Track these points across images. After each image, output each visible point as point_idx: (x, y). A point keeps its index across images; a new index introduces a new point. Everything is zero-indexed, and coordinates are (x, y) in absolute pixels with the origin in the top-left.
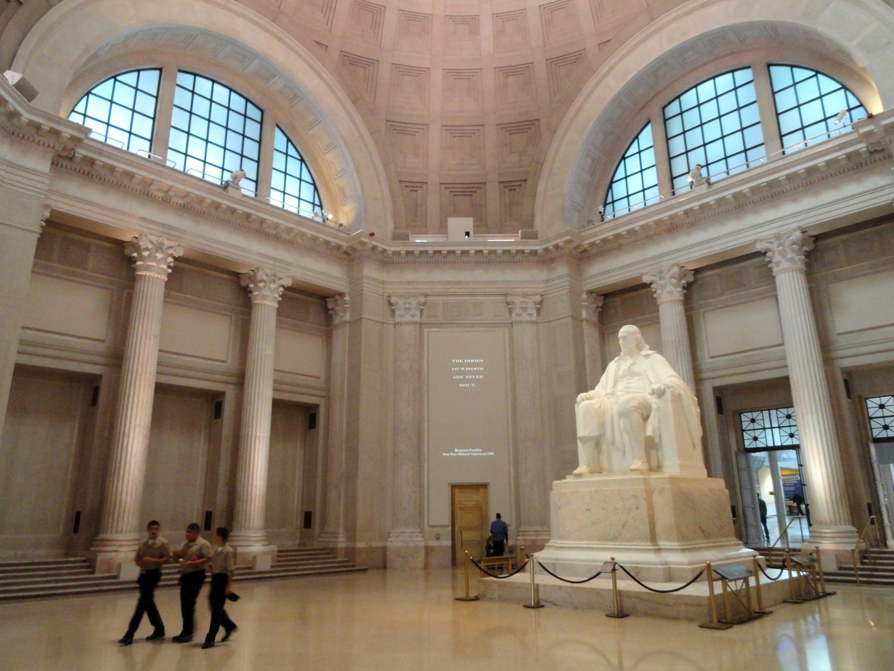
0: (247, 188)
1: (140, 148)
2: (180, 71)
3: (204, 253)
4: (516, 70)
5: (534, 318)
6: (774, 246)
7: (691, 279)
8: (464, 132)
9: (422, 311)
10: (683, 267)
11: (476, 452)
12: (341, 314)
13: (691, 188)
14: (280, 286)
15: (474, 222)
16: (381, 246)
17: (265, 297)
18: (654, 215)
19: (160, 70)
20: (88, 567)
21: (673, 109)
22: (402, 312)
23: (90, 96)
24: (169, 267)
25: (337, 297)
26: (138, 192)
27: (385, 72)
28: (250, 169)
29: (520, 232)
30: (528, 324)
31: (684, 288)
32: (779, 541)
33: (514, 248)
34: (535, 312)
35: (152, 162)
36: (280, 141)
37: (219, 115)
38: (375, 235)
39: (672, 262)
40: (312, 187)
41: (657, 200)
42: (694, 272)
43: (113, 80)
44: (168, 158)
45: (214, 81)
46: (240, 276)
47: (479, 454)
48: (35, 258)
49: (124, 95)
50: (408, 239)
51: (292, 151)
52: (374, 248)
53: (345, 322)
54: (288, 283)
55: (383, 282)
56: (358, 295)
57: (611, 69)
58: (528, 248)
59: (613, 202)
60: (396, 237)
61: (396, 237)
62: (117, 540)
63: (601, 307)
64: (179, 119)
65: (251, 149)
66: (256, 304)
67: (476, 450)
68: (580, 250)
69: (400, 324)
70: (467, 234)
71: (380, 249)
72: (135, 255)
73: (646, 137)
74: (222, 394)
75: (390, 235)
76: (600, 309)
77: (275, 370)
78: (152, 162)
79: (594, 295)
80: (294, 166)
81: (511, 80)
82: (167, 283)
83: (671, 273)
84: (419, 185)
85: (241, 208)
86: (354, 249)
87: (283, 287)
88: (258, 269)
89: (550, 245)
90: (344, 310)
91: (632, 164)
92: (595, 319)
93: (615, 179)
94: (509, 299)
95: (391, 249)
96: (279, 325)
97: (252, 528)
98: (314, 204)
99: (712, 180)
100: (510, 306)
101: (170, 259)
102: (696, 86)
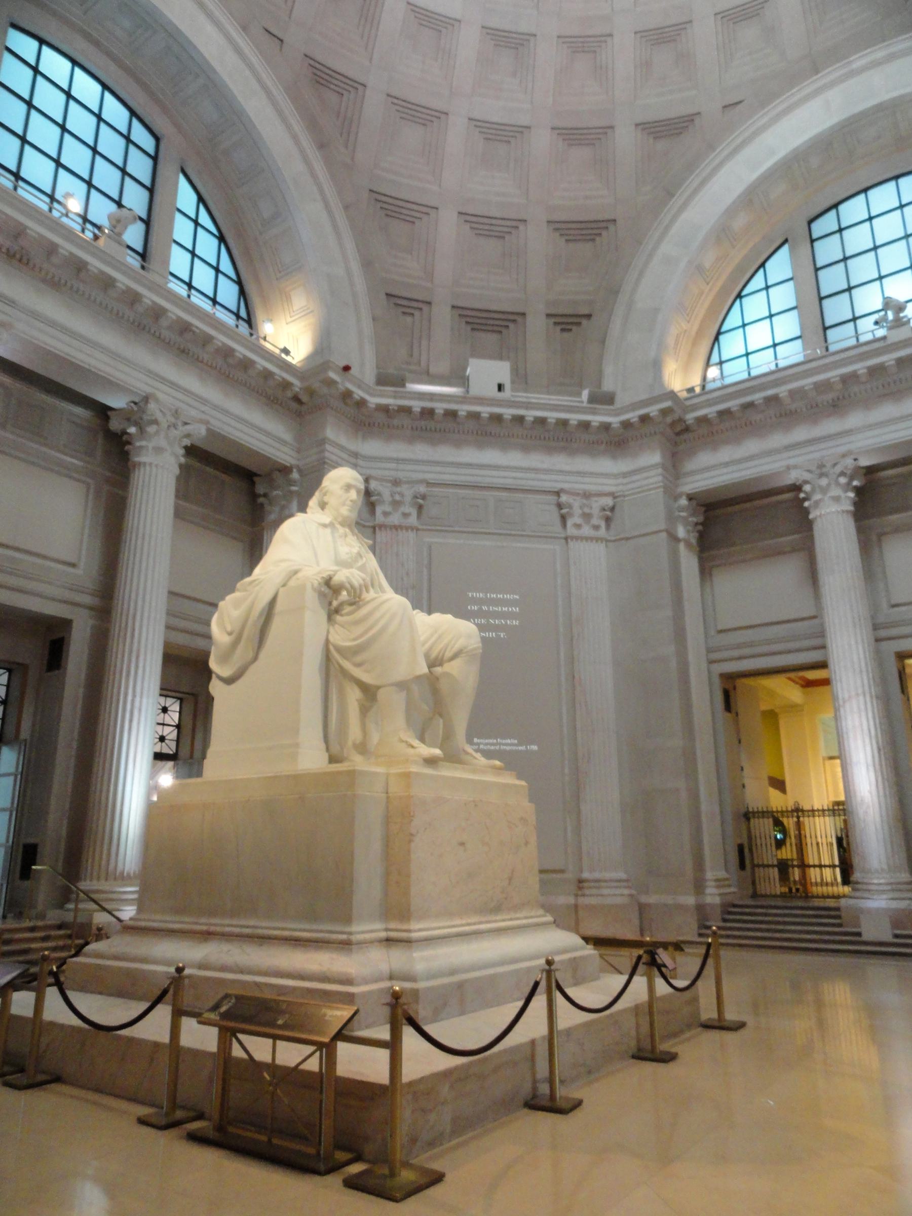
5: (602, 532)
8: (492, 228)
12: (283, 503)
16: (358, 393)
17: (159, 450)
18: (812, 375)
21: (827, 223)
22: (388, 509)
25: (276, 475)
32: (245, 1056)
33: (574, 418)
36: (186, 198)
41: (799, 358)
45: (75, 63)
46: (109, 413)
47: (514, 748)
50: (404, 386)
51: (204, 219)
52: (347, 395)
58: (596, 419)
59: (721, 363)
60: (382, 380)
61: (382, 380)
63: (702, 524)
65: (135, 199)
67: (509, 741)
68: (678, 429)
69: (382, 526)
76: (700, 528)
79: (694, 503)
80: (208, 246)
83: (838, 469)
86: (311, 393)
88: (146, 399)
89: (633, 416)
91: (754, 306)
92: (694, 541)
93: (724, 329)
94: (564, 498)
102: (865, 190)
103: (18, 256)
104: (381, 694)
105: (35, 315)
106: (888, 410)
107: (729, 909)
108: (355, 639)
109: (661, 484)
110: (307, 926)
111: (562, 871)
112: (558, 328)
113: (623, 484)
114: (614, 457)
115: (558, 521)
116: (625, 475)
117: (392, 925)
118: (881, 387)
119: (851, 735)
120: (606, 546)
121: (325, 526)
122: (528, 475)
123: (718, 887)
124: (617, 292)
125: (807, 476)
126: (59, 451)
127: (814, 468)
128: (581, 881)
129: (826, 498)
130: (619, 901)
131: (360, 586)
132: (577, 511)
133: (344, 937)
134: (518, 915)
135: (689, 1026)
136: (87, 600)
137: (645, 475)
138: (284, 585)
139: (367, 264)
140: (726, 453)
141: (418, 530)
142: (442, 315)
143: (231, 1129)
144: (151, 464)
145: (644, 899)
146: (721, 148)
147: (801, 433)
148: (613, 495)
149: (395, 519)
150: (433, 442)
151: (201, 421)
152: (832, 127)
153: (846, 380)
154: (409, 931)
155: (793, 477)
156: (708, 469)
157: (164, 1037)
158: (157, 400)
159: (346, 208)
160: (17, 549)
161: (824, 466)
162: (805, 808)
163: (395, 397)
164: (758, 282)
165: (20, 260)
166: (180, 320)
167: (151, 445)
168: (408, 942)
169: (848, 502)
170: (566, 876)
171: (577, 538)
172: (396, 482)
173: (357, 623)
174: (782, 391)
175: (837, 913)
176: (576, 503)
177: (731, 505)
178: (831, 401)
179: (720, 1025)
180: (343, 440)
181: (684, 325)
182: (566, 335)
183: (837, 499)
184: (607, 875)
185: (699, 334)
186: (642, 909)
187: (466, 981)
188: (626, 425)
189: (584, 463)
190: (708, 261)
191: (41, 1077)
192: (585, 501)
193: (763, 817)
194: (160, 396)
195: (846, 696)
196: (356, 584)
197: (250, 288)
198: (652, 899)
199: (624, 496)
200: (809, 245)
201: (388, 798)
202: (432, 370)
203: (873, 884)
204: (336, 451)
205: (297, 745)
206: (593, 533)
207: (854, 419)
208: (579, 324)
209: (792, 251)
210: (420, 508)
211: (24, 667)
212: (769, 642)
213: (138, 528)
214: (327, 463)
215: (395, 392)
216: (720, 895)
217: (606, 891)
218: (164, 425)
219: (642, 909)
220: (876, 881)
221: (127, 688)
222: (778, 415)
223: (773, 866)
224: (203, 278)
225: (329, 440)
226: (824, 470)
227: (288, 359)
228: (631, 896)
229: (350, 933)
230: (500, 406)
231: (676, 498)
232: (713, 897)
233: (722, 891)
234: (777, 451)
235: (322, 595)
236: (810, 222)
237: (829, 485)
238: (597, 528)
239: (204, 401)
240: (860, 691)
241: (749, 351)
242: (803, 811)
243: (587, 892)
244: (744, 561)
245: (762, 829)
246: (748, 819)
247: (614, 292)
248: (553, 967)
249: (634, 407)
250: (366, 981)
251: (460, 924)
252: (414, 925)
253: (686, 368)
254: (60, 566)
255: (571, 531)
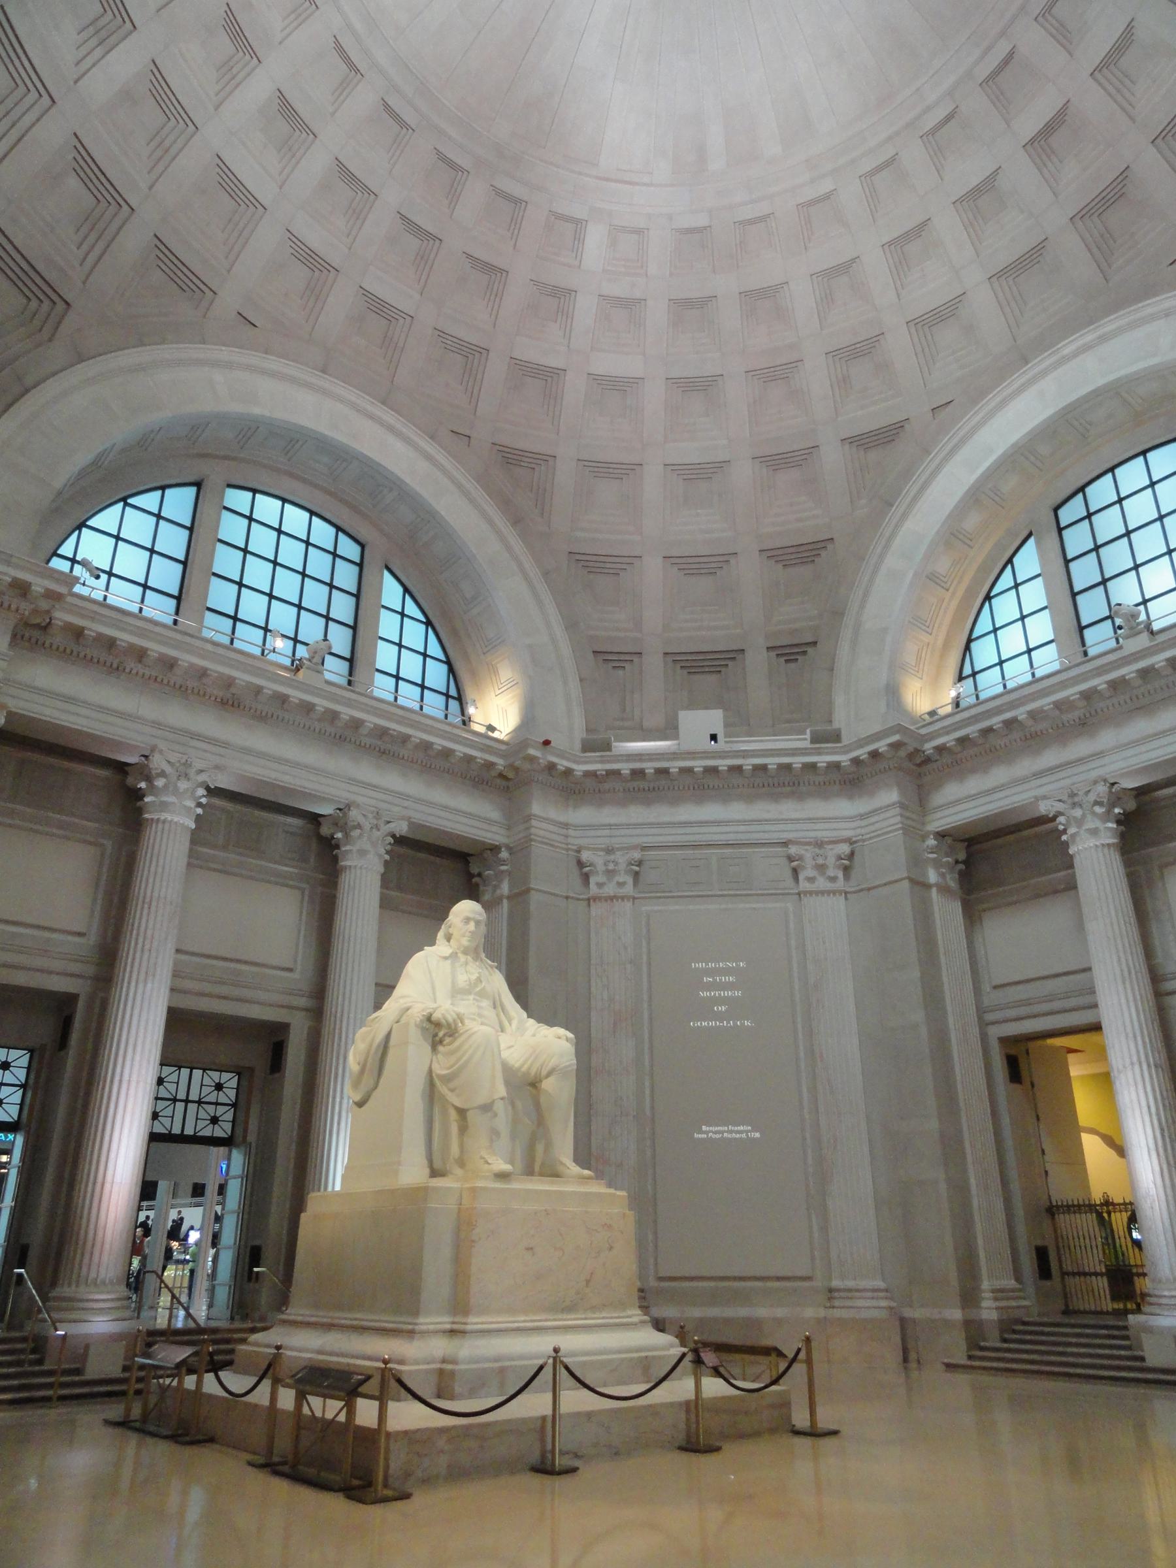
0: (335, 669)
1: (159, 609)
2: (230, 486)
3: (253, 778)
4: (95, 181)
5: (840, 884)
6: (367, 826)
7: (1131, 805)
9: (637, 874)
10: (1113, 784)
11: (742, 1131)
13: (1118, 642)
14: (386, 836)
15: (725, 717)
16: (563, 764)
17: (362, 853)
19: (198, 485)
20: (33, 1351)
23: (84, 530)
24: (199, 805)
26: (213, 698)
27: (565, 475)
28: (340, 639)
29: (808, 731)
30: (829, 895)
31: (1119, 822)
32: (310, 1413)
33: (797, 761)
34: (840, 875)
35: (181, 632)
36: (391, 592)
37: (291, 553)
38: (552, 744)
39: (1094, 774)
40: (445, 668)
41: (1056, 666)
42: (1134, 793)
43: (121, 504)
44: (205, 624)
45: (312, 513)
48: (382, 887)
49: (137, 526)
51: (411, 609)
52: (551, 767)
53: (501, 898)
54: (402, 828)
55: (566, 826)
56: (521, 850)
57: (230, 365)
58: (822, 760)
59: (974, 674)
60: (587, 747)
61: (587, 747)
62: (88, 1300)
63: (964, 862)
64: (226, 561)
65: (343, 608)
66: (345, 867)
69: (596, 899)
70: (714, 737)
71: (578, 773)
72: (143, 785)
73: (1028, 561)
74: (283, 1028)
75: (578, 745)
76: (962, 866)
77: (377, 984)
78: (181, 632)
79: (949, 840)
80: (415, 634)
81: (73, 182)
82: (194, 833)
83: (1092, 797)
84: (627, 657)
85: (321, 703)
87: (393, 836)
88: (348, 806)
89: (862, 753)
90: (499, 875)
91: (1006, 608)
92: (953, 885)
94: (793, 850)
95: (580, 768)
96: (385, 903)
97: (95, 1283)
98: (447, 696)
99: (1156, 626)
100: (795, 863)
101: (201, 791)
103: (230, 702)
104: (470, 1114)
105: (247, 751)
106: (1141, 726)
107: (1010, 1327)
108: (449, 1068)
109: (900, 825)
110: (392, 1319)
111: (809, 1278)
112: (782, 660)
113: (861, 827)
114: (851, 797)
115: (788, 873)
116: (862, 817)
117: (457, 1319)
118: (1128, 701)
119: (1129, 1112)
120: (846, 899)
121: (446, 958)
122: (752, 828)
123: (996, 1299)
124: (842, 614)
125: (1060, 807)
126: (275, 863)
127: (1065, 798)
128: (831, 1290)
129: (1082, 832)
130: (875, 1314)
131: (454, 1021)
132: (809, 862)
133: (410, 1327)
134: (569, 1317)
135: (773, 1431)
136: (303, 1002)
137: (882, 816)
138: (397, 1022)
139: (571, 626)
140: (974, 784)
141: (634, 898)
142: (654, 664)
143: (301, 1467)
144: (355, 867)
145: (908, 1313)
146: (936, 451)
147: (1050, 757)
148: (849, 841)
149: (610, 890)
150: (648, 803)
151: (403, 818)
152: (1050, 418)
153: (1087, 696)
154: (465, 1324)
155: (1044, 808)
156: (958, 802)
157: (266, 1402)
158: (358, 806)
159: (546, 574)
160: (238, 961)
161: (1076, 795)
162: (1116, 1201)
163: (602, 762)
164: (1006, 580)
165: (233, 705)
166: (377, 727)
167: (355, 848)
168: (463, 1332)
169: (1109, 834)
170: (814, 1284)
171: (811, 893)
172: (609, 851)
173: (452, 1053)
174: (1021, 713)
175: (1124, 1333)
176: (808, 853)
177: (998, 837)
178: (1077, 720)
179: (814, 1433)
180: (553, 813)
181: (925, 638)
182: (792, 665)
183: (1094, 832)
184: (863, 1284)
185: (946, 645)
186: (903, 1322)
187: (507, 1367)
188: (856, 761)
189: (816, 808)
190: (943, 565)
191: (201, 1437)
192: (817, 851)
193: (1069, 1213)
194: (360, 799)
195: (1121, 1067)
196: (450, 1020)
197: (458, 666)
198: (917, 1313)
199: (864, 841)
200: (1055, 534)
201: (459, 1208)
202: (646, 724)
203: (1165, 1296)
204: (544, 825)
205: (399, 1163)
206: (829, 886)
207: (1107, 738)
208: (805, 653)
209: (1038, 543)
210: (636, 875)
211: (251, 1070)
212: (1050, 998)
213: (344, 932)
214: (535, 841)
215: (602, 756)
216: (997, 1308)
217: (860, 1303)
218: (367, 826)
219: (903, 1322)
220: (1166, 1293)
221: (335, 1091)
222: (1023, 738)
223: (1101, 1274)
224: (411, 666)
225: (535, 815)
226: (1076, 799)
227: (496, 735)
228: (891, 1308)
229: (416, 1324)
230: (714, 758)
231: (924, 838)
232: (988, 1311)
233: (998, 1304)
234: (1024, 780)
235: (424, 1030)
236: (1056, 510)
237: (1084, 816)
238: (833, 879)
239: (408, 797)
240: (1135, 1059)
241: (1003, 658)
242: (1113, 1204)
243: (837, 1303)
244: (1009, 904)
245: (1085, 1229)
246: (1053, 1215)
247: (838, 614)
248: (559, 1354)
249: (861, 743)
250: (417, 1362)
251: (522, 1320)
252: (472, 1319)
253: (935, 682)
254: (279, 973)
255: (804, 885)
